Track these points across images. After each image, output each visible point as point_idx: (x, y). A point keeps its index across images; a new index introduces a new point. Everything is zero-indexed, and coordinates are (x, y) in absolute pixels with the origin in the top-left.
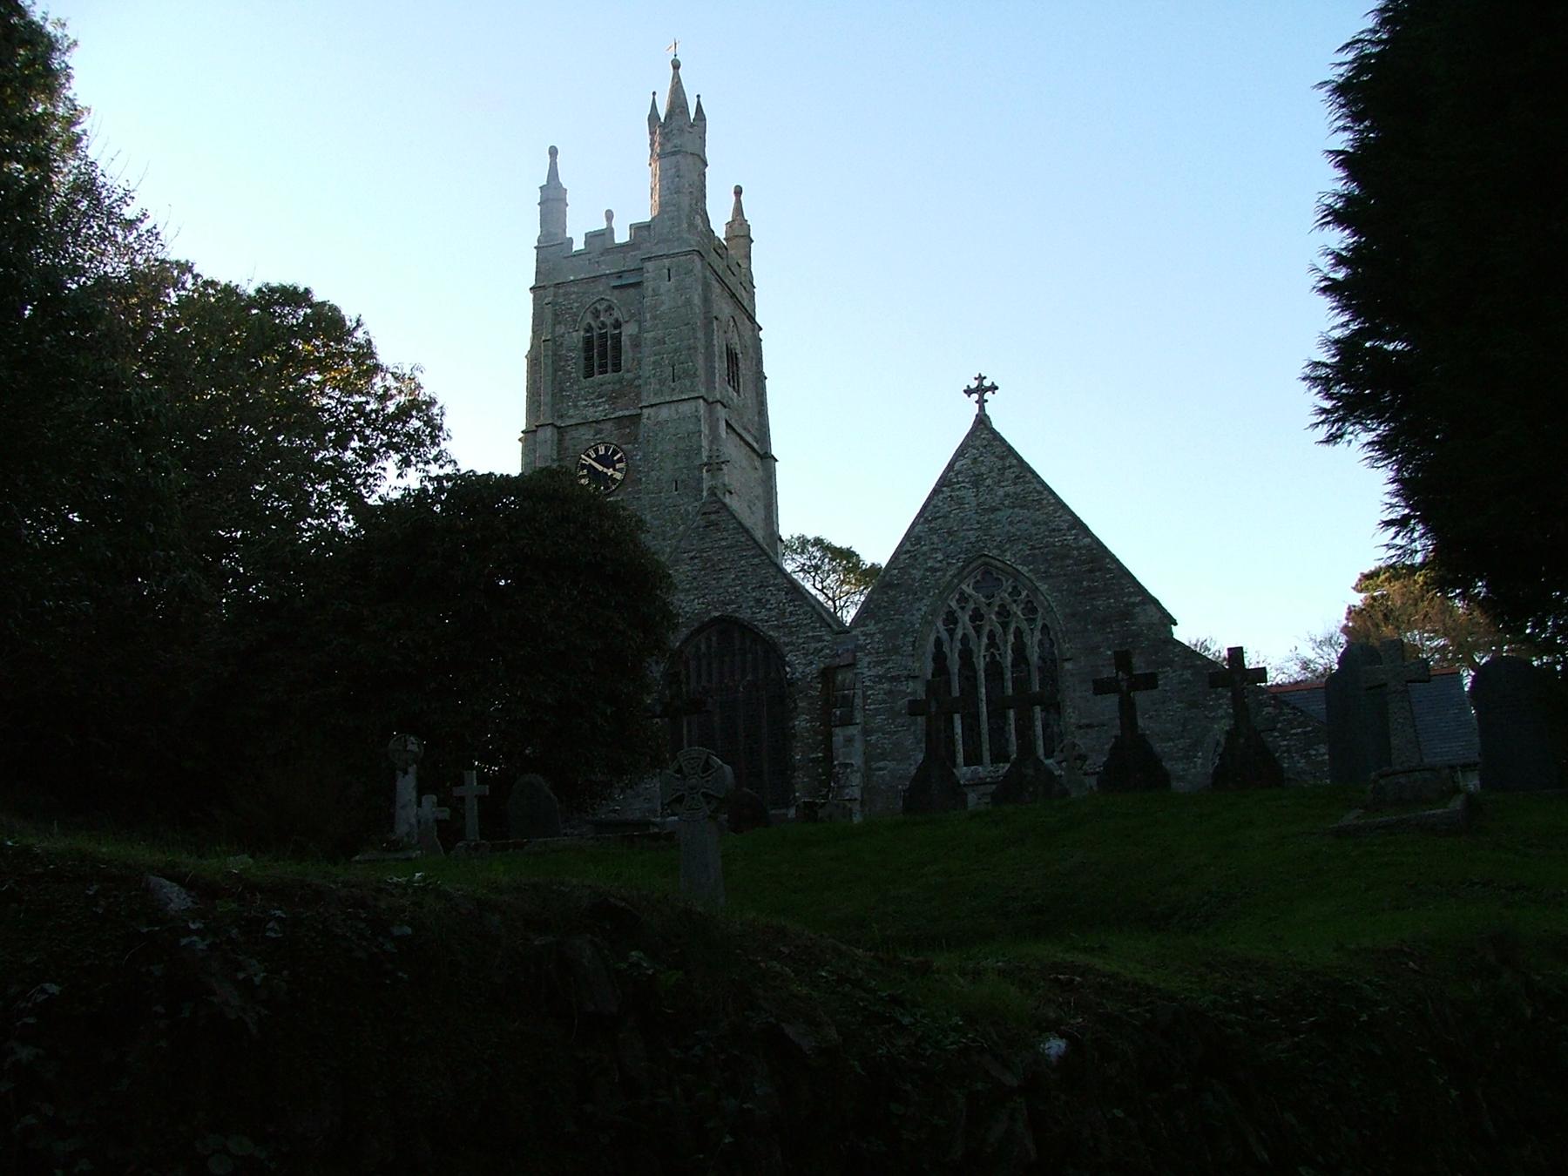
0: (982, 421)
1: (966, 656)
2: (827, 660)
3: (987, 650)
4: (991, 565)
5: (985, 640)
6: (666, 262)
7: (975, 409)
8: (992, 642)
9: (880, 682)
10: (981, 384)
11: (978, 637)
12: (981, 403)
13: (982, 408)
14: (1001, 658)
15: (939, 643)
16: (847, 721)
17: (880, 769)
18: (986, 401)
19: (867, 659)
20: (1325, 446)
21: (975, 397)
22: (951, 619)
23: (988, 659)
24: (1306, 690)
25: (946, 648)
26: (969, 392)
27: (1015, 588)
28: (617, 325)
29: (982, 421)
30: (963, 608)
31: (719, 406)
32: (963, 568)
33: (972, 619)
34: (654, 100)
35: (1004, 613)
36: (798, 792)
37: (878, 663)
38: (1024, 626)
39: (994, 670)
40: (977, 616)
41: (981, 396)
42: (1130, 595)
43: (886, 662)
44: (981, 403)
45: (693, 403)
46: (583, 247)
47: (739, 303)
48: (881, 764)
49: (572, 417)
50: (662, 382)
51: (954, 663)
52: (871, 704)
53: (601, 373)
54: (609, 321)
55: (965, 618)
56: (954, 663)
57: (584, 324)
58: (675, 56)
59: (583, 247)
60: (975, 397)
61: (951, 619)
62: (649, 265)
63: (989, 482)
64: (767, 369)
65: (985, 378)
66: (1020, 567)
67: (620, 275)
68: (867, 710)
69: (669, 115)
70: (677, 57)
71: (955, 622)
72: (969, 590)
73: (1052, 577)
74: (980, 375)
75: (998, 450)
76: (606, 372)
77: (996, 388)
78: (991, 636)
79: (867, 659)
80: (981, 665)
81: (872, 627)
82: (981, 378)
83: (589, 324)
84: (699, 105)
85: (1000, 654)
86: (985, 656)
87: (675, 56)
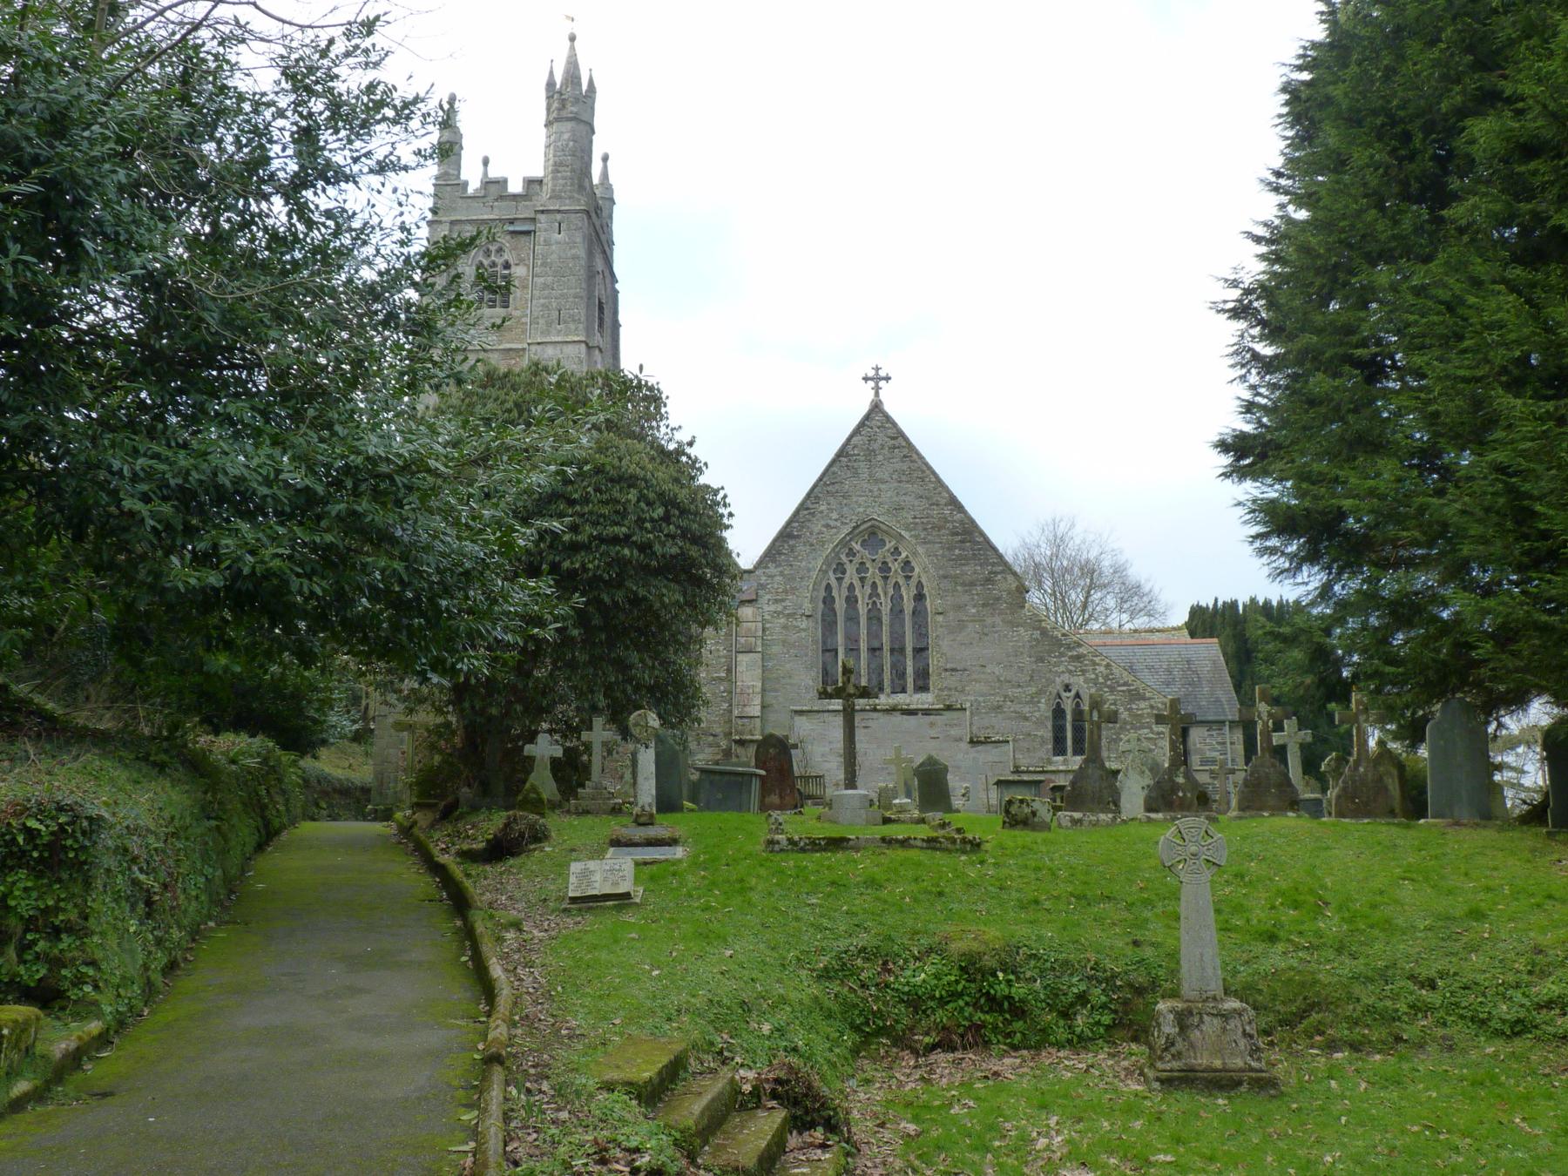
0: (876, 407)
1: (851, 600)
3: (870, 598)
4: (879, 528)
6: (559, 217)
10: (877, 374)
12: (877, 389)
13: (877, 394)
19: (768, 597)
21: (871, 384)
22: (840, 569)
24: (1185, 751)
25: (835, 593)
26: (866, 379)
28: (507, 266)
29: (876, 407)
31: (597, 352)
32: (855, 528)
33: (858, 571)
35: (885, 568)
37: (776, 601)
38: (901, 581)
39: (874, 616)
40: (862, 567)
41: (877, 384)
42: (993, 564)
43: (783, 600)
44: (877, 389)
45: (577, 346)
47: (604, 252)
50: (549, 324)
51: (840, 605)
53: (490, 307)
54: (500, 261)
55: (851, 570)
56: (908, 605)
62: (542, 217)
63: (880, 458)
64: (622, 318)
67: (512, 222)
69: (565, 82)
71: (844, 572)
73: (929, 542)
75: (891, 432)
76: (494, 307)
79: (768, 597)
80: (862, 609)
81: (772, 569)
82: (877, 369)
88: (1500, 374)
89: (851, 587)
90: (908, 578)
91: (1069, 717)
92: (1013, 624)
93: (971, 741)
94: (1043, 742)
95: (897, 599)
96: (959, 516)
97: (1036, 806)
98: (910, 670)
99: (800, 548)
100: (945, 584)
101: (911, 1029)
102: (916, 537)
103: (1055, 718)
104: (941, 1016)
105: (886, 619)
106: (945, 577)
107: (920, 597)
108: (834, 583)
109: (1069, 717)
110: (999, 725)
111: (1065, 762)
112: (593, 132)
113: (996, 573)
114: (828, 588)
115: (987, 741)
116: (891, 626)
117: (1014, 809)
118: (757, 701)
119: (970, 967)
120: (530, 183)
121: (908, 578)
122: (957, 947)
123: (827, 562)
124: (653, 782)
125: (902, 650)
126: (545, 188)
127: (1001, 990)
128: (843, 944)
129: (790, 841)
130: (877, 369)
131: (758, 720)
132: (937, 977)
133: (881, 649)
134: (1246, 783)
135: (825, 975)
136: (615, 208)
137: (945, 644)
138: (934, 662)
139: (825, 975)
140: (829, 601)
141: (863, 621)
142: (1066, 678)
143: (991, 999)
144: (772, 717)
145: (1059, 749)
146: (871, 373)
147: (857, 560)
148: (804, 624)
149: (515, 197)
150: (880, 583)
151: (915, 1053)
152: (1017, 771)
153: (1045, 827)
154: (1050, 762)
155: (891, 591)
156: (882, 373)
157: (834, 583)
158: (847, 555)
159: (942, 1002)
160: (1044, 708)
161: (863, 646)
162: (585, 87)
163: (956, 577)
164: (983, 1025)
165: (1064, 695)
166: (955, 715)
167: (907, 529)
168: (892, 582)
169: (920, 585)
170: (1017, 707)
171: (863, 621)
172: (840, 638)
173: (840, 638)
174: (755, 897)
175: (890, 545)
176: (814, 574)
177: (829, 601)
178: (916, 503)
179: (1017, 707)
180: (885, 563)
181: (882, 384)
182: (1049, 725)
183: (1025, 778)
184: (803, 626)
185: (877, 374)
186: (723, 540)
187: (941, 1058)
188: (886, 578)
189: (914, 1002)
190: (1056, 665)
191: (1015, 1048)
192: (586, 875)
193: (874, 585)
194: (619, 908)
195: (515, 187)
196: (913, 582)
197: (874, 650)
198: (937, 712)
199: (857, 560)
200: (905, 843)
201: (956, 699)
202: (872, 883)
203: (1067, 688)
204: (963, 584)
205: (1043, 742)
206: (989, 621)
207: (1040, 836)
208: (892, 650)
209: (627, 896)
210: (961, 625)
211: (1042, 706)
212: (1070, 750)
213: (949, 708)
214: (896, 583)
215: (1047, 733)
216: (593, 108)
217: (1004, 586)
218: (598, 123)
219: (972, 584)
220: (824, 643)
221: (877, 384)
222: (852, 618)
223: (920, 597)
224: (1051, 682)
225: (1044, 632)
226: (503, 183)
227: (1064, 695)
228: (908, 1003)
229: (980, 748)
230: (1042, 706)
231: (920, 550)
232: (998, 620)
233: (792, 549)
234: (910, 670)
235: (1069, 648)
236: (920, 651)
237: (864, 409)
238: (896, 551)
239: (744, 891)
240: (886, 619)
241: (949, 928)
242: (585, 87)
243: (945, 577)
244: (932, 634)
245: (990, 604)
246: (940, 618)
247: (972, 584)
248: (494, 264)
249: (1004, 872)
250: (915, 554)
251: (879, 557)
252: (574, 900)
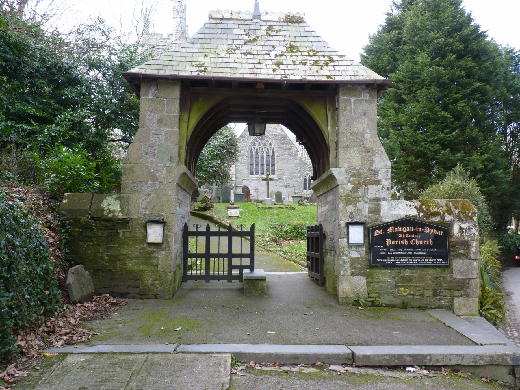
1: (257, 153)
8: (262, 151)
22: (254, 145)
25: (253, 151)
33: (259, 146)
35: (265, 145)
38: (269, 148)
39: (262, 157)
40: (260, 145)
42: (291, 145)
51: (254, 154)
56: (271, 154)
71: (255, 146)
80: (259, 155)
88: (391, 125)
89: (257, 149)
90: (271, 147)
91: (307, 181)
92: (295, 159)
93: (285, 187)
94: (302, 187)
95: (268, 153)
96: (283, 133)
97: (304, 201)
98: (271, 170)
99: (245, 140)
100: (279, 149)
101: (286, 237)
102: (273, 138)
103: (304, 181)
104: (290, 235)
105: (265, 157)
106: (279, 148)
107: (273, 152)
108: (253, 148)
109: (307, 181)
110: (291, 183)
111: (306, 192)
113: (291, 147)
114: (251, 149)
115: (288, 187)
116: (266, 159)
117: (300, 202)
118: (235, 176)
119: (295, 227)
121: (271, 147)
122: (293, 224)
123: (251, 143)
124: (233, 197)
125: (269, 165)
126: (173, 37)
127: (300, 231)
128: (275, 224)
129: (262, 207)
131: (235, 181)
132: (290, 229)
133: (264, 164)
135: (272, 228)
137: (279, 164)
138: (276, 168)
139: (272, 228)
140: (251, 152)
141: (260, 158)
142: (307, 172)
143: (298, 232)
144: (238, 180)
145: (305, 188)
147: (258, 143)
148: (246, 158)
150: (264, 149)
151: (286, 240)
152: (295, 194)
153: (306, 205)
154: (303, 192)
155: (266, 151)
157: (253, 148)
159: (291, 233)
160: (302, 179)
161: (260, 164)
163: (282, 148)
164: (296, 237)
165: (307, 176)
166: (281, 180)
167: (271, 136)
168: (267, 148)
169: (273, 149)
170: (296, 179)
171: (260, 158)
172: (254, 162)
173: (254, 162)
174: (259, 216)
175: (266, 139)
176: (248, 146)
177: (251, 152)
179: (296, 179)
180: (265, 144)
182: (303, 183)
183: (297, 195)
184: (245, 158)
187: (291, 241)
188: (265, 147)
189: (286, 233)
190: (305, 169)
191: (302, 240)
192: (231, 213)
193: (262, 149)
194: (237, 218)
196: (272, 148)
197: (262, 165)
198: (277, 180)
199: (258, 143)
200: (282, 208)
201: (282, 177)
202: (277, 214)
203: (307, 175)
204: (284, 149)
205: (302, 187)
206: (290, 158)
207: (305, 207)
208: (267, 165)
209: (238, 216)
210: (283, 159)
211: (301, 179)
212: (307, 189)
213: (280, 179)
214: (268, 149)
215: (302, 185)
217: (293, 150)
219: (286, 149)
220: (250, 163)
222: (257, 157)
223: (273, 152)
224: (304, 173)
225: (302, 161)
227: (307, 176)
228: (285, 233)
229: (287, 188)
230: (301, 179)
231: (274, 141)
232: (292, 158)
233: (243, 140)
234: (271, 170)
235: (308, 165)
236: (273, 165)
238: (268, 141)
239: (257, 215)
240: (265, 157)
241: (291, 221)
243: (279, 148)
244: (276, 161)
245: (290, 154)
246: (278, 157)
247: (286, 149)
249: (300, 213)
250: (272, 142)
251: (264, 142)
252: (229, 217)
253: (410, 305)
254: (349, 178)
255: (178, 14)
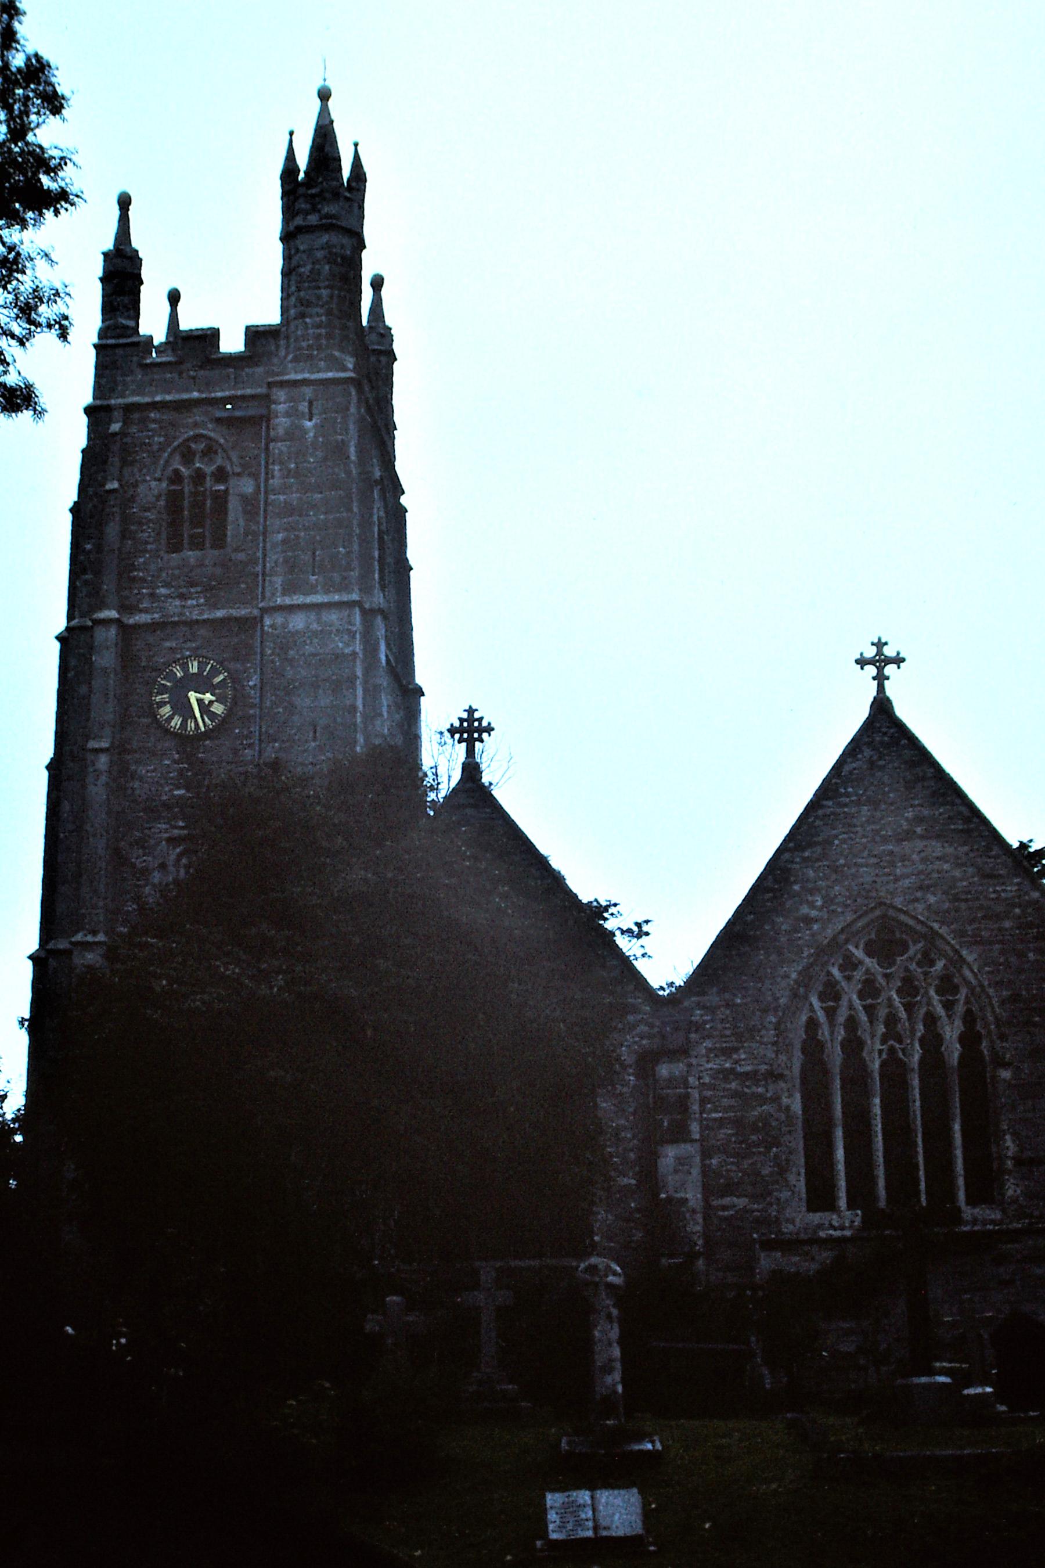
0: (882, 707)
1: (853, 1045)
2: (644, 1042)
5: (881, 1029)
7: (871, 690)
8: (892, 1033)
9: (726, 1079)
10: (880, 653)
11: (871, 1022)
12: (881, 679)
13: (881, 688)
14: (904, 1054)
15: (812, 1024)
16: (679, 1134)
17: (724, 1208)
18: (888, 678)
20: (617, 902)
21: (871, 670)
22: (831, 993)
23: (884, 1056)
25: (824, 1033)
26: (862, 662)
27: (926, 954)
29: (882, 707)
30: (848, 979)
34: (291, 142)
36: (597, 1235)
40: (869, 989)
41: (880, 670)
44: (881, 679)
46: (242, 349)
48: (727, 1201)
49: (146, 611)
51: (835, 1056)
52: (711, 1111)
55: (851, 995)
56: (835, 1056)
57: (169, 471)
58: (325, 80)
59: (242, 349)
60: (871, 670)
61: (831, 993)
65: (886, 644)
66: (936, 926)
68: (706, 1119)
70: (327, 83)
71: (837, 998)
72: (859, 953)
74: (879, 639)
77: (857, 662)
78: (891, 1020)
82: (880, 645)
83: (176, 472)
84: (357, 160)
85: (903, 1050)
86: (880, 1052)
87: (325, 80)
112: (362, 246)
120: (255, 335)
123: (806, 978)
130: (880, 645)
134: (943, 1006)
136: (396, 366)
146: (871, 652)
147: (858, 975)
149: (231, 360)
156: (889, 652)
158: (842, 968)
162: (346, 173)
178: (957, 873)
181: (890, 670)
185: (880, 653)
186: (615, 941)
195: (232, 343)
199: (858, 975)
216: (361, 208)
218: (370, 230)
221: (880, 670)
226: (210, 337)
237: (861, 713)
242: (346, 173)
248: (199, 477)
253: (44, 122)
254: (792, 1103)
255: (228, 763)
